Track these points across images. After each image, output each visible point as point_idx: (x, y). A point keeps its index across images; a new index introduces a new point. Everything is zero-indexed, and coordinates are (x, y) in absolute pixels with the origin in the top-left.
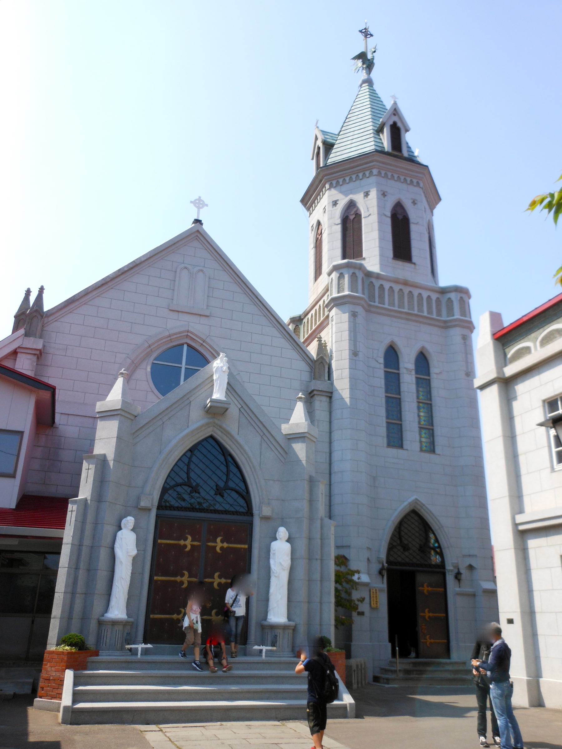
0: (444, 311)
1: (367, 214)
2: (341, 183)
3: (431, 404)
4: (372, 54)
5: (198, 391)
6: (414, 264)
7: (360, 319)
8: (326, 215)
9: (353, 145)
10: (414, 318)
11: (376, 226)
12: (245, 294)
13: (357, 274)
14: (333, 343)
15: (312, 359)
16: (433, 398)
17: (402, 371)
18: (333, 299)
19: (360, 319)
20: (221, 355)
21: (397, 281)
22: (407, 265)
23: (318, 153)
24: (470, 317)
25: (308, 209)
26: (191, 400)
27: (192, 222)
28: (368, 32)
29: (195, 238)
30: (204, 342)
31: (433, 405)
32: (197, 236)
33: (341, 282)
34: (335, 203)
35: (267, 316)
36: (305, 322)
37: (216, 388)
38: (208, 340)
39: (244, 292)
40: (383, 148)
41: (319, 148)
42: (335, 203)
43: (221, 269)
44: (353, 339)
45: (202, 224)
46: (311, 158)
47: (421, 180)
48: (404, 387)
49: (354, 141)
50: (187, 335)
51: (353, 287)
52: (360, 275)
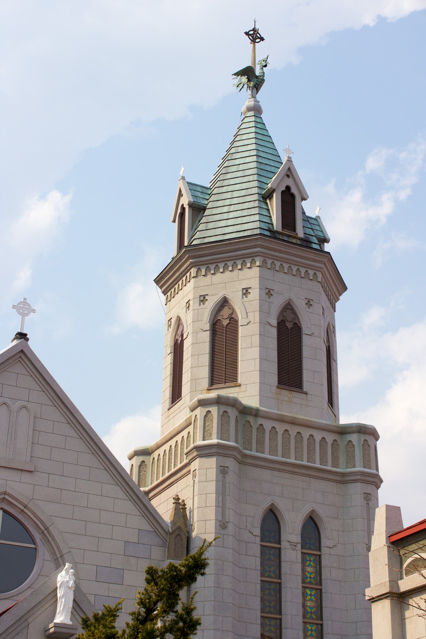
0: (342, 459)
1: (245, 322)
3: (321, 590)
4: (262, 69)
5: (38, 610)
6: (306, 393)
7: (231, 477)
8: (190, 313)
9: (231, 215)
11: (256, 339)
13: (230, 414)
14: (195, 495)
15: (167, 530)
16: (323, 581)
17: (284, 545)
18: (197, 448)
19: (231, 477)
20: (67, 566)
21: (281, 419)
22: (297, 397)
23: (182, 215)
24: (377, 469)
25: (165, 293)
26: (29, 621)
27: (13, 337)
29: (18, 360)
30: (25, 507)
31: (323, 591)
32: (20, 357)
33: (207, 424)
34: (203, 299)
35: (109, 471)
36: (154, 458)
37: (60, 607)
38: (30, 505)
39: (80, 436)
40: (270, 226)
41: (183, 208)
42: (203, 299)
43: (51, 404)
44: (221, 505)
45: (27, 340)
46: (172, 219)
48: (285, 568)
49: (232, 208)
50: (4, 498)
51: (222, 435)
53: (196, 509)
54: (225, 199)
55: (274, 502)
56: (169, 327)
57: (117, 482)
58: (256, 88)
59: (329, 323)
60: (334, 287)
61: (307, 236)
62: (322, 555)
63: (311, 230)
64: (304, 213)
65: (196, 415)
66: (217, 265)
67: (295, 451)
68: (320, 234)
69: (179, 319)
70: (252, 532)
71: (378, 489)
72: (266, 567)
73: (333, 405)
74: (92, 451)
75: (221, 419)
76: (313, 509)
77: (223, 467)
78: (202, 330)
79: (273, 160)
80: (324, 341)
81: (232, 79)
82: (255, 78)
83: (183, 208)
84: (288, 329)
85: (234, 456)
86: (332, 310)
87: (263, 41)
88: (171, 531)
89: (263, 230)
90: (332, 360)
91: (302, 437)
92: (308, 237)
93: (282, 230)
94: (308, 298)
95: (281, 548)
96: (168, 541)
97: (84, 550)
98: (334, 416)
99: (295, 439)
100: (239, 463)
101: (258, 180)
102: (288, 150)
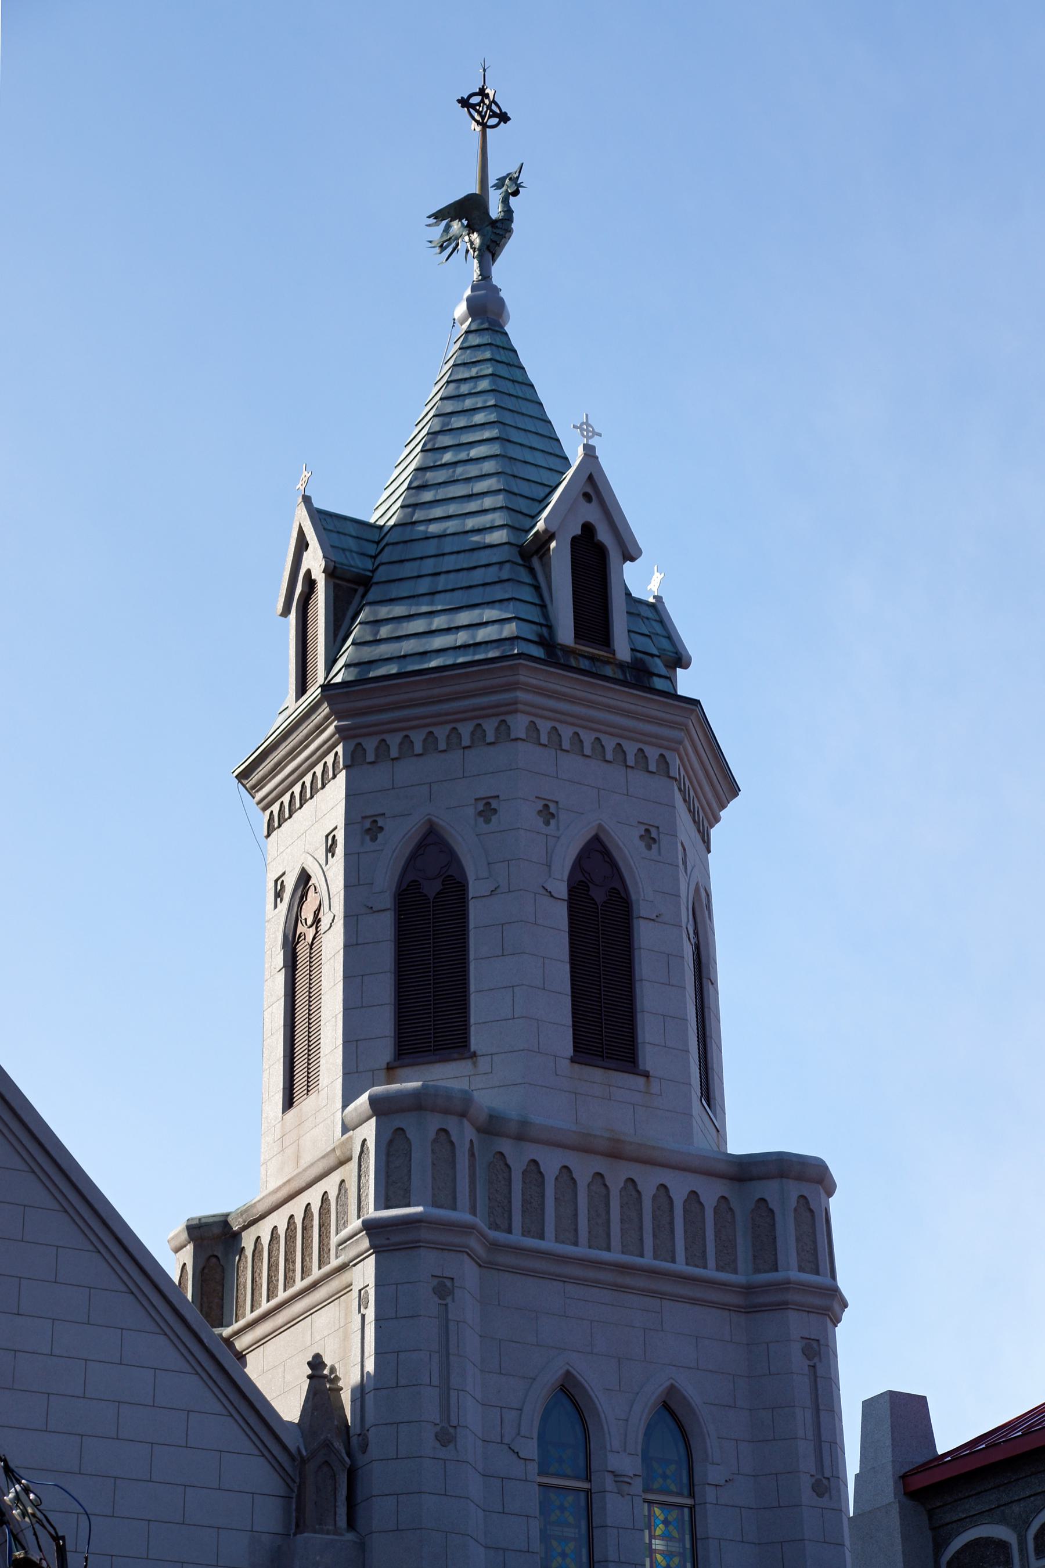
2: (394, 753)
6: (646, 1075)
10: (641, 1282)
12: (66, 1211)
21: (584, 1148)
24: (834, 1276)
28: (494, 107)
47: (676, 750)
52: (465, 1134)
53: (372, 1393)
54: (421, 558)
55: (571, 1369)
56: (279, 900)
57: (162, 1324)
58: (490, 251)
59: (697, 884)
60: (707, 788)
61: (639, 655)
62: (697, 1507)
63: (647, 640)
64: (628, 594)
65: (365, 1140)
66: (407, 736)
67: (622, 1229)
68: (665, 644)
69: (304, 878)
70: (516, 1451)
71: (837, 1326)
72: (554, 1543)
73: (712, 1102)
74: (94, 1245)
75: (432, 1150)
76: (672, 1385)
77: (441, 1279)
78: (372, 908)
79: (543, 451)
80: (689, 934)
81: (427, 225)
82: (487, 226)
83: (310, 584)
84: (596, 904)
85: (467, 1250)
86: (702, 846)
87: (505, 123)
88: (304, 1453)
89: (526, 642)
90: (704, 980)
91: (638, 1192)
92: (642, 661)
93: (576, 643)
94: (645, 822)
95: (591, 1490)
96: (298, 1480)
97: (76, 1515)
98: (714, 1130)
99: (621, 1196)
100: (480, 1266)
101: (507, 508)
102: (586, 428)
